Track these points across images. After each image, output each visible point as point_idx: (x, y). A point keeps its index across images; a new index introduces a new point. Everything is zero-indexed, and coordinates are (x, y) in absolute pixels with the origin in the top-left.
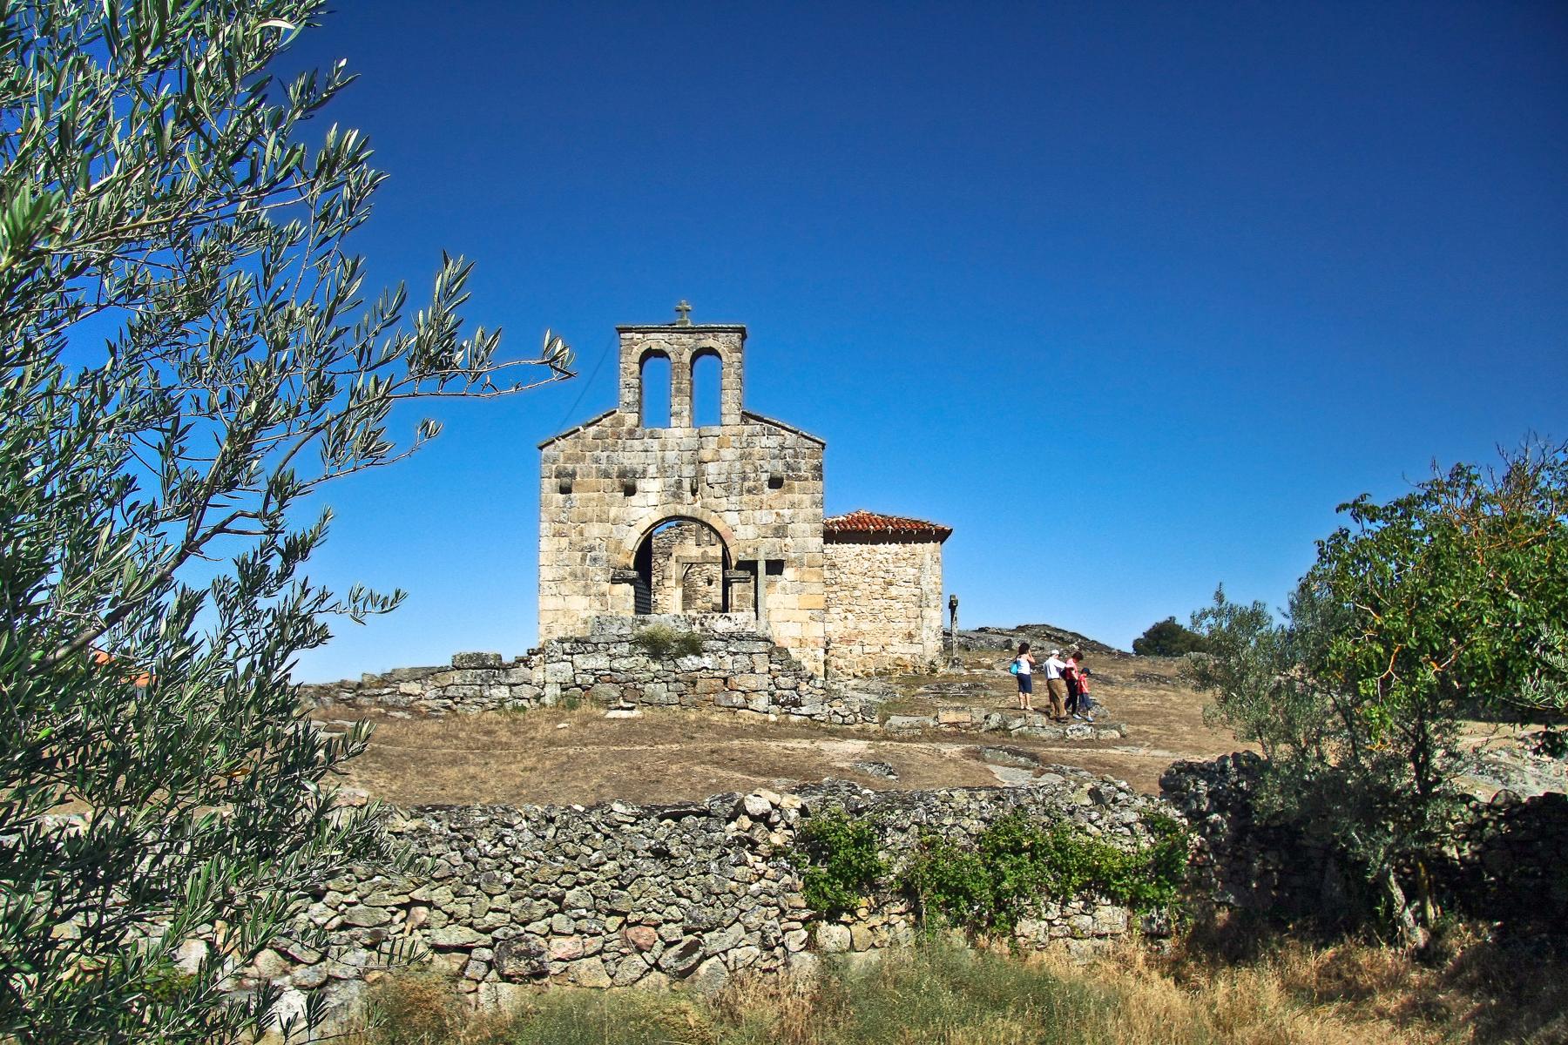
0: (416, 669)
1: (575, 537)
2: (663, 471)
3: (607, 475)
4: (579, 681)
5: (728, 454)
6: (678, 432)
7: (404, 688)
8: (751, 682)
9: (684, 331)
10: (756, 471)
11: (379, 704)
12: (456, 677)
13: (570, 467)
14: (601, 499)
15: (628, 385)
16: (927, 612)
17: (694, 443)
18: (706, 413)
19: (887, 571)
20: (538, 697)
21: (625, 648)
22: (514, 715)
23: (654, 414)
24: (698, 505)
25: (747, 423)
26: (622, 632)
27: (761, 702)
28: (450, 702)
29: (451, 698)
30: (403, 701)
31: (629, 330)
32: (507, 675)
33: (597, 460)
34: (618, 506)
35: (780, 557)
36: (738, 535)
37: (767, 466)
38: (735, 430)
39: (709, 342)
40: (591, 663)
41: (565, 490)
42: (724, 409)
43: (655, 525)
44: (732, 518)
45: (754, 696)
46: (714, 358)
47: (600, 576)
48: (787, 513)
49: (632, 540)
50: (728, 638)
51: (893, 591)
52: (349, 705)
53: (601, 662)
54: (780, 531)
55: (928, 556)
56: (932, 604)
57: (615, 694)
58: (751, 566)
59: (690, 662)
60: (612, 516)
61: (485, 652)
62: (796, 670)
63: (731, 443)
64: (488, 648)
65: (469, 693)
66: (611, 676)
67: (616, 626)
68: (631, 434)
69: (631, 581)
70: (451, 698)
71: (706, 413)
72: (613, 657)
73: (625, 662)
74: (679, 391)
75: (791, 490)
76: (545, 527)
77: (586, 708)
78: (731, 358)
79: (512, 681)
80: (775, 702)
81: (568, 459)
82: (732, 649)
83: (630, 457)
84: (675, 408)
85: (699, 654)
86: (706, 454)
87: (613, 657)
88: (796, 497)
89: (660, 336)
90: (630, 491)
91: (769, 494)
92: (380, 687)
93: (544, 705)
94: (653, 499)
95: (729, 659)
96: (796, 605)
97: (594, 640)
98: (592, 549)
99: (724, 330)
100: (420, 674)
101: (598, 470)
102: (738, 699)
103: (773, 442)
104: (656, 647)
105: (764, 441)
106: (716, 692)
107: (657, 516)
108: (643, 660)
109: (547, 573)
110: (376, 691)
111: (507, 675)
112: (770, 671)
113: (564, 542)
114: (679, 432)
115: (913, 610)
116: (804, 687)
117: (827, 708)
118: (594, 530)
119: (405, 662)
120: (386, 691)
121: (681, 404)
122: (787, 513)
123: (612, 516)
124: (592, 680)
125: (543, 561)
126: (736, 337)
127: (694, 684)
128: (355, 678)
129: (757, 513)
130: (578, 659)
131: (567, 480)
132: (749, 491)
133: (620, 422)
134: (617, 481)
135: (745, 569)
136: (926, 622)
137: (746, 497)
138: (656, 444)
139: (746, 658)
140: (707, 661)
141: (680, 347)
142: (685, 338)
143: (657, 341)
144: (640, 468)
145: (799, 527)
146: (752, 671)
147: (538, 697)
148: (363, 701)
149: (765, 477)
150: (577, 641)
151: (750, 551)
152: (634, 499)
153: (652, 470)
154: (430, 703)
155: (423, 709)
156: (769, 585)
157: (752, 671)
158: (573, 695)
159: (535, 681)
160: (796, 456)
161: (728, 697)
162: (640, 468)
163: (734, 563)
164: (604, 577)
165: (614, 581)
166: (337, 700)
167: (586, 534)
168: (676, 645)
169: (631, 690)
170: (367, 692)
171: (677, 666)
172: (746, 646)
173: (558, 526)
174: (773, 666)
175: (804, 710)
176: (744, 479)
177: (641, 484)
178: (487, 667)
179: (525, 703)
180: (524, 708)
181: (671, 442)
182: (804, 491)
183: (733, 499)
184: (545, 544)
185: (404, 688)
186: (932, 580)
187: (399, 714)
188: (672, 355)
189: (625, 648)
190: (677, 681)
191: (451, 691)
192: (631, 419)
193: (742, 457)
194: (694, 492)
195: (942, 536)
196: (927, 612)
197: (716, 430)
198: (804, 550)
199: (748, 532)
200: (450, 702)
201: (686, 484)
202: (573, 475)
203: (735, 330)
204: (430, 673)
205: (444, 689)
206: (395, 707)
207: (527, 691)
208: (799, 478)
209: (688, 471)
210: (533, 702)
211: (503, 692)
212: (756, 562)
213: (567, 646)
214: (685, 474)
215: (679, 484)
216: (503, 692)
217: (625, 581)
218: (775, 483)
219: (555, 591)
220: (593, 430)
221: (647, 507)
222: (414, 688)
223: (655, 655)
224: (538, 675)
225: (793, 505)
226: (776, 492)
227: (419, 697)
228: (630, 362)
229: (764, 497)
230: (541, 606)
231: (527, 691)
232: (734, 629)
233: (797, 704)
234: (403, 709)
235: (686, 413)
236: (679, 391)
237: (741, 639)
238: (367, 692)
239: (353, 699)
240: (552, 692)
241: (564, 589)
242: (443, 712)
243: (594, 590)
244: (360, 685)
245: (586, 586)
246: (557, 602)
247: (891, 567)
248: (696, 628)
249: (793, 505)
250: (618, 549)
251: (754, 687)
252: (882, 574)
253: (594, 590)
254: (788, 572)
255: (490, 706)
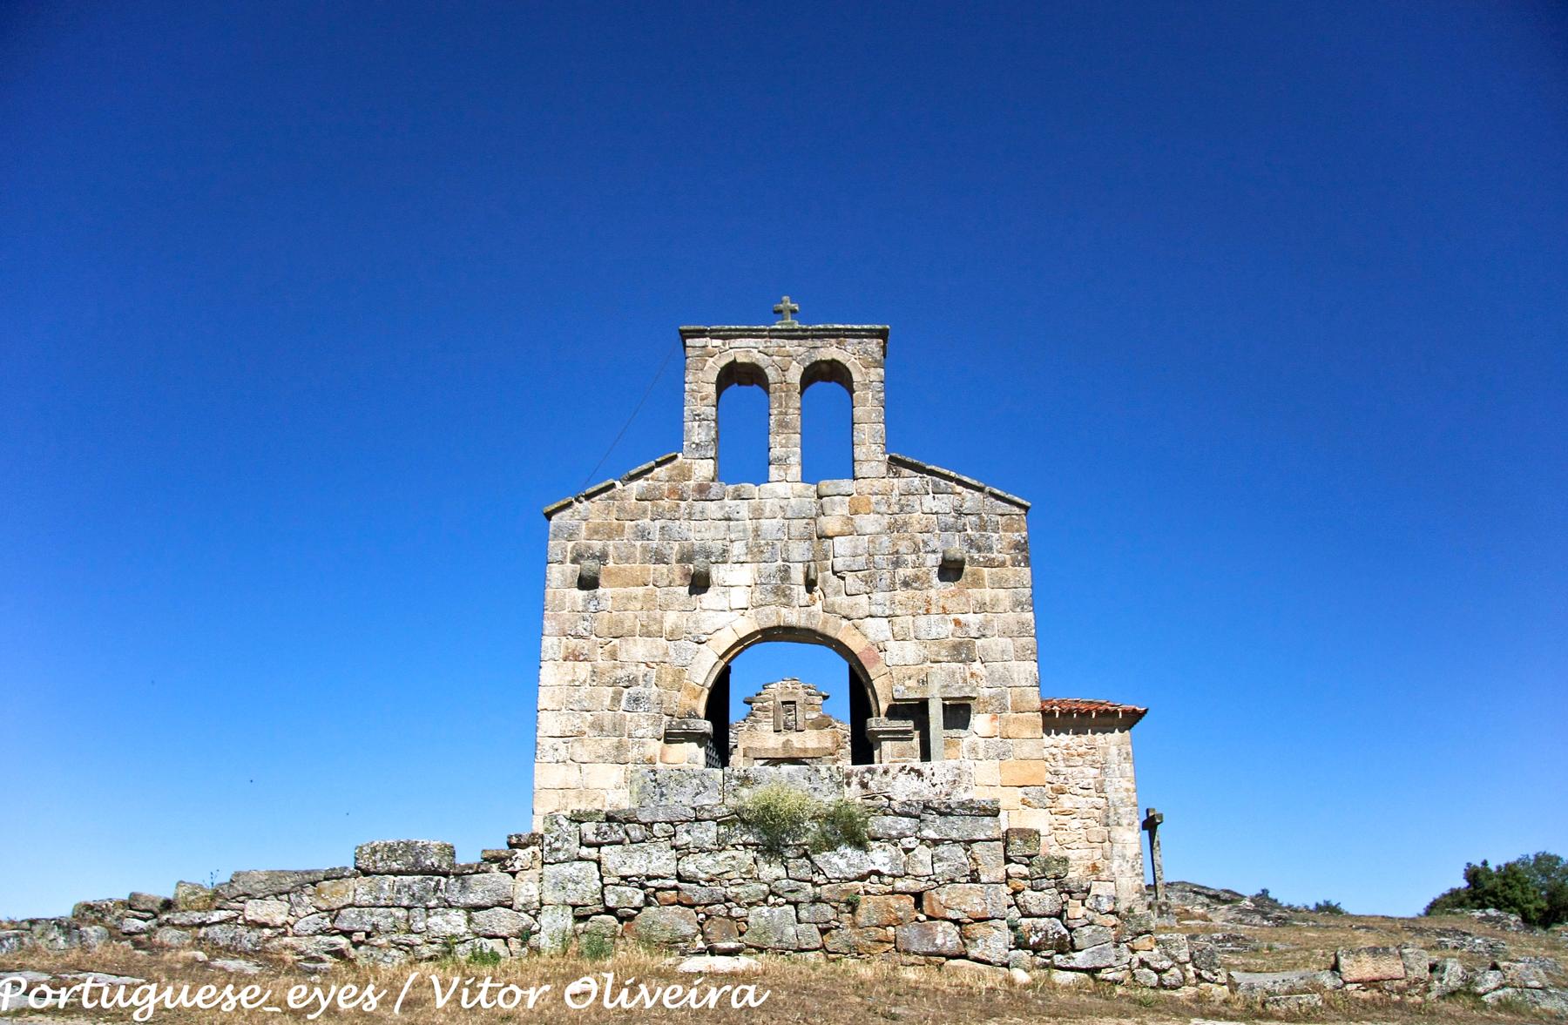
0: (284, 874)
1: (602, 663)
2: (756, 553)
3: (660, 559)
4: (611, 901)
5: (869, 523)
6: (781, 489)
7: (254, 910)
8: (971, 900)
9: (790, 335)
10: (916, 550)
11: (198, 943)
12: (360, 890)
13: (597, 545)
14: (649, 598)
15: (697, 417)
16: (1118, 833)
17: (810, 505)
18: (828, 458)
19: (1056, 773)
20: (525, 935)
21: (708, 833)
22: (474, 969)
23: (743, 460)
24: (819, 606)
25: (897, 475)
26: (703, 800)
27: (995, 942)
28: (342, 942)
29: (347, 934)
30: (249, 938)
31: (700, 334)
32: (464, 888)
33: (643, 534)
34: (678, 608)
35: (967, 692)
36: (888, 658)
37: (935, 543)
38: (879, 485)
39: (829, 351)
40: (637, 865)
41: (587, 583)
42: (859, 452)
43: (744, 643)
44: (877, 629)
45: (979, 929)
46: (833, 387)
47: (645, 727)
48: (973, 619)
49: (703, 671)
50: (920, 811)
51: (1066, 802)
52: (138, 945)
53: (659, 861)
54: (962, 651)
55: (1114, 750)
56: (1124, 822)
57: (689, 929)
58: (916, 711)
59: (843, 860)
60: (667, 626)
61: (422, 840)
62: (1052, 874)
63: (881, 504)
64: (430, 837)
65: (385, 924)
66: (677, 891)
67: (690, 790)
68: (702, 491)
69: (699, 738)
70: (347, 934)
71: (828, 458)
72: (681, 851)
73: (707, 861)
74: (783, 425)
75: (977, 582)
76: (551, 644)
77: (629, 953)
78: (867, 376)
79: (473, 899)
80: (1020, 944)
81: (594, 532)
82: (929, 833)
83: (701, 532)
84: (776, 452)
85: (860, 845)
86: (830, 524)
87: (681, 851)
88: (987, 594)
89: (751, 342)
90: (699, 584)
91: (939, 590)
92: (208, 909)
93: (537, 950)
94: (740, 598)
95: (923, 853)
96: (997, 779)
97: (645, 817)
98: (631, 682)
99: (855, 334)
100: (288, 884)
101: (645, 550)
102: (945, 936)
103: (944, 503)
104: (771, 832)
105: (929, 502)
106: (899, 922)
107: (746, 626)
108: (747, 856)
109: (549, 724)
110: (197, 917)
111: (464, 888)
112: (1008, 876)
113: (583, 670)
114: (785, 486)
115: (1098, 830)
116: (1076, 910)
117: (1127, 955)
118: (638, 649)
119: (261, 861)
120: (217, 916)
121: (786, 446)
122: (973, 619)
123: (667, 626)
124: (638, 898)
125: (544, 700)
126: (874, 345)
127: (853, 906)
128: (159, 888)
129: (922, 621)
130: (610, 855)
131: (590, 565)
132: (906, 584)
133: (685, 474)
134: (677, 568)
135: (905, 718)
136: (1117, 848)
137: (901, 594)
138: (744, 508)
139: (959, 850)
140: (880, 858)
141: (785, 361)
142: (790, 346)
143: (745, 350)
144: (717, 546)
145: (995, 644)
146: (974, 878)
147: (525, 935)
148: (168, 936)
149: (933, 561)
150: (610, 819)
151: (912, 683)
152: (709, 598)
153: (738, 550)
154: (306, 944)
155: (289, 956)
156: (949, 743)
157: (974, 878)
158: (603, 924)
159: (519, 901)
160: (982, 527)
161: (927, 934)
162: (717, 546)
163: (884, 707)
164: (650, 731)
165: (670, 738)
166: (115, 934)
167: (622, 656)
168: (814, 827)
169: (718, 920)
170: (179, 918)
171: (818, 870)
172: (959, 827)
173: (573, 642)
174: (1013, 869)
175: (1080, 959)
176: (897, 564)
177: (718, 573)
178: (435, 872)
179: (497, 945)
180: (495, 957)
181: (770, 505)
182: (1000, 584)
183: (878, 596)
184: (551, 674)
185: (254, 910)
186: (1121, 784)
187: (233, 965)
188: (772, 374)
189: (708, 833)
190: (817, 900)
191: (348, 919)
192: (704, 469)
193: (893, 528)
194: (810, 585)
195: (1132, 719)
196: (1118, 833)
197: (846, 485)
198: (1005, 681)
199: (903, 653)
200: (342, 942)
201: (797, 574)
202: (603, 557)
203: (872, 334)
204: (312, 881)
205: (334, 914)
206: (230, 950)
207: (504, 922)
208: (990, 563)
209: (799, 551)
210: (515, 944)
211: (456, 922)
212: (923, 704)
213: (589, 829)
214: (795, 556)
215: (785, 574)
216: (456, 922)
217: (689, 737)
218: (951, 570)
219: (563, 754)
220: (637, 486)
221: (731, 610)
222: (273, 911)
223: (771, 849)
224: (526, 889)
225: (981, 607)
226: (952, 587)
227: (282, 930)
228: (701, 383)
229: (932, 593)
230: (539, 781)
231: (504, 922)
232: (928, 793)
233: (1065, 946)
234: (246, 955)
235: (795, 460)
236: (783, 425)
237: (945, 812)
238: (179, 918)
239: (150, 932)
240: (554, 924)
241: (580, 752)
242: (330, 962)
243: (633, 754)
244: (168, 905)
245: (619, 747)
246: (570, 775)
247: (1061, 767)
248: (853, 793)
249: (981, 607)
250: (678, 681)
251: (978, 910)
252: (1048, 777)
253: (633, 754)
254: (980, 722)
255: (426, 951)
